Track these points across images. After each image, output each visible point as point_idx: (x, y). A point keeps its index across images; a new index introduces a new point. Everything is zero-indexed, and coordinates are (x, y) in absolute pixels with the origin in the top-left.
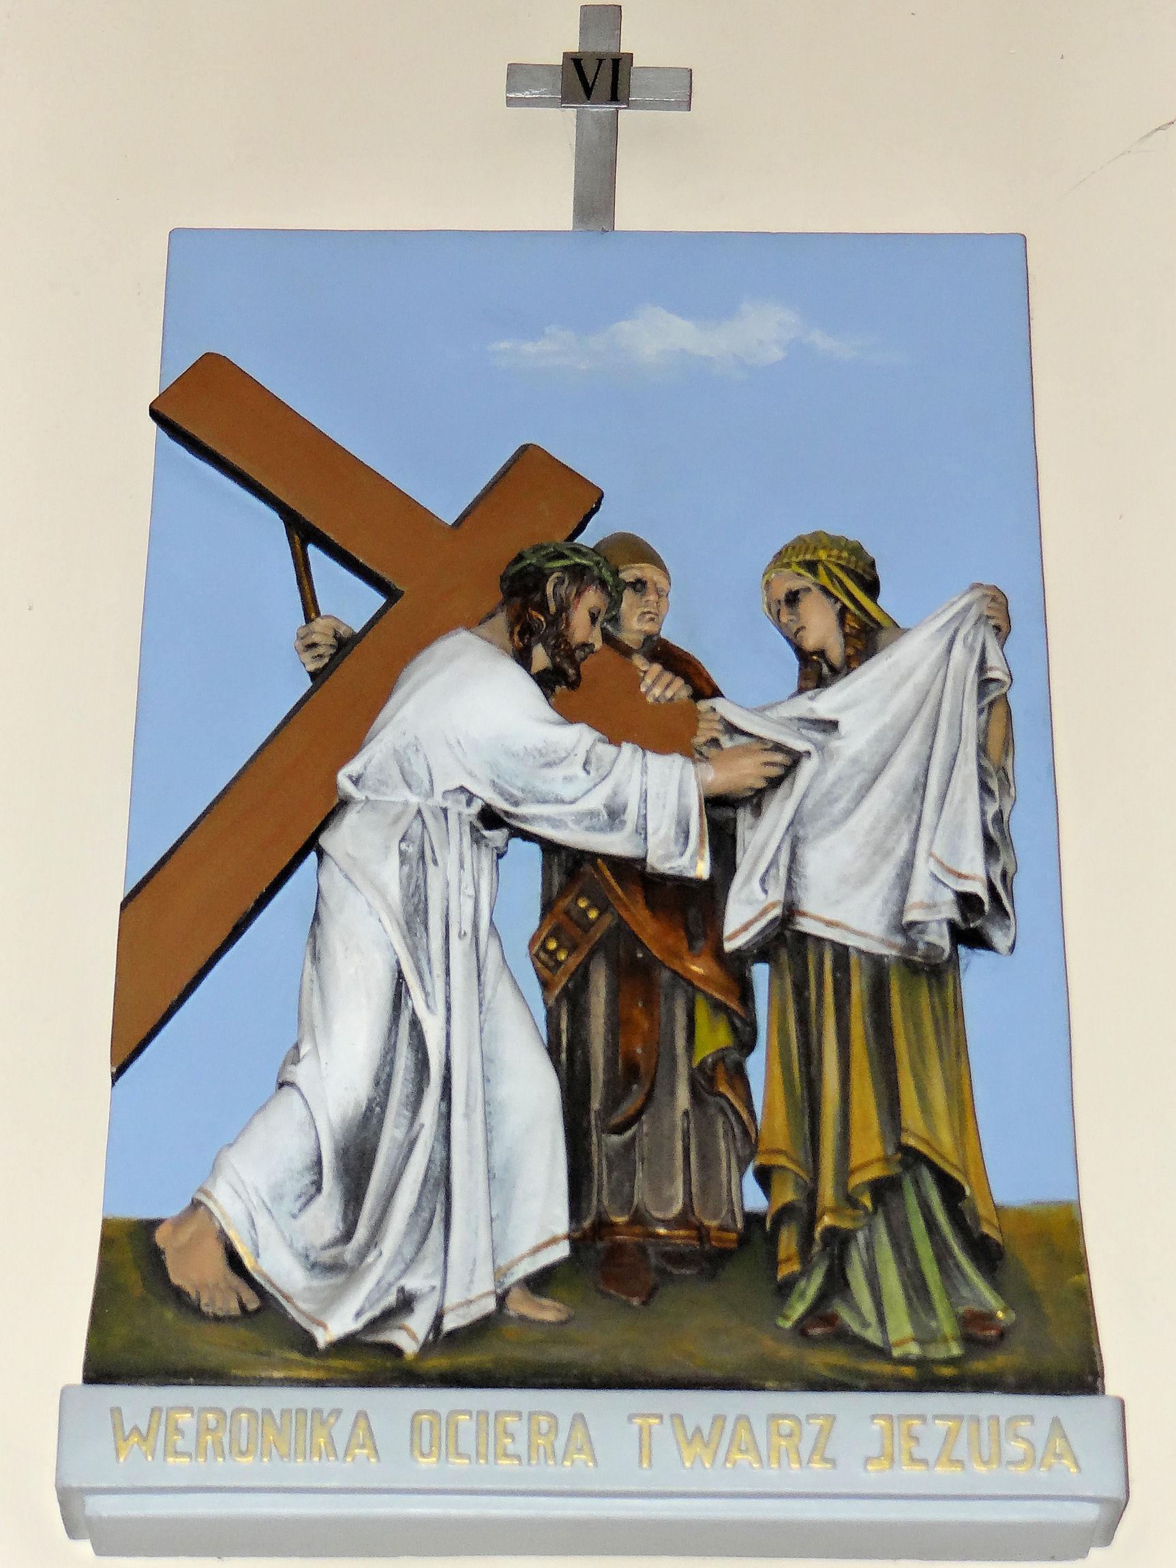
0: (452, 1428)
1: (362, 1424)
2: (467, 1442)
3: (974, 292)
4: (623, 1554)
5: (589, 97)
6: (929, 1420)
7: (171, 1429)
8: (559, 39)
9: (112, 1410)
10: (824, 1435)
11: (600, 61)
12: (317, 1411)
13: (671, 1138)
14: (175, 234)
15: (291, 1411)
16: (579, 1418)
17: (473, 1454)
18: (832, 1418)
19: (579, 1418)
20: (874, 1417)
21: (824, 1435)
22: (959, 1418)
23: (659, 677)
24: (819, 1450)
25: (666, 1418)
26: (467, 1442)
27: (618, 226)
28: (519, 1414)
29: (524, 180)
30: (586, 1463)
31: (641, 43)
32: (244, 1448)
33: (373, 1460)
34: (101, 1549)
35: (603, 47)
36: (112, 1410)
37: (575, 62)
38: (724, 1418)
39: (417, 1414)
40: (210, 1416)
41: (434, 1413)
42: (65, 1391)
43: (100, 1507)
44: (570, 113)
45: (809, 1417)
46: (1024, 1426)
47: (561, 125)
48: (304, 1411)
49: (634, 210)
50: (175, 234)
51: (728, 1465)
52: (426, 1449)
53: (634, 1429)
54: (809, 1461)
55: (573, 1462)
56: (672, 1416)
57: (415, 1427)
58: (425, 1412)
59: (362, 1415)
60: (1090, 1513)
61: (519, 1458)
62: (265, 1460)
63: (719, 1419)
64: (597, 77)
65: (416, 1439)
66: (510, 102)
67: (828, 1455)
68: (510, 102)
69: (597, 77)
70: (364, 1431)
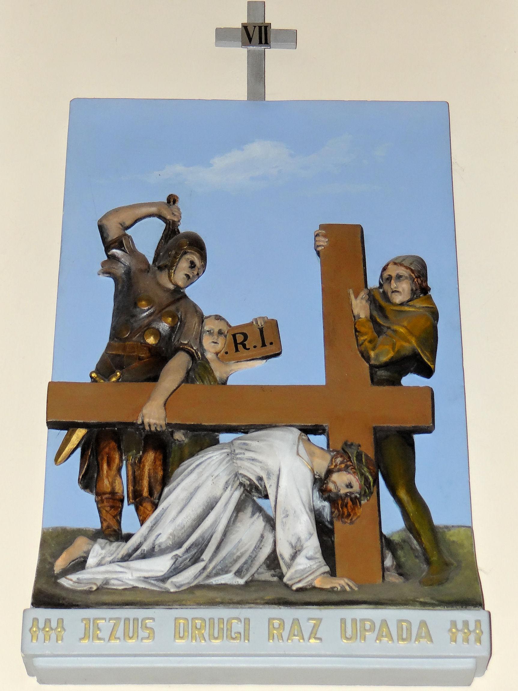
1: (48, 624)
7: (194, 628)
8: (238, 19)
9: (342, 619)
10: (315, 628)
11: (255, 27)
12: (136, 620)
15: (89, 620)
17: (122, 638)
18: (320, 620)
19: (296, 621)
20: (310, 619)
21: (315, 628)
22: (118, 619)
24: (313, 634)
29: (225, 76)
31: (275, 20)
32: (181, 635)
33: (301, 641)
34: (41, 681)
35: (259, 21)
36: (342, 619)
37: (245, 27)
40: (181, 621)
41: (186, 619)
42: (25, 611)
43: (40, 662)
44: (244, 51)
47: (240, 54)
48: (129, 619)
49: (276, 89)
51: (378, 641)
52: (216, 635)
53: (83, 624)
54: (309, 639)
55: (292, 640)
57: (176, 627)
58: (277, 619)
59: (296, 621)
60: (469, 664)
64: (257, 34)
67: (317, 636)
69: (257, 34)
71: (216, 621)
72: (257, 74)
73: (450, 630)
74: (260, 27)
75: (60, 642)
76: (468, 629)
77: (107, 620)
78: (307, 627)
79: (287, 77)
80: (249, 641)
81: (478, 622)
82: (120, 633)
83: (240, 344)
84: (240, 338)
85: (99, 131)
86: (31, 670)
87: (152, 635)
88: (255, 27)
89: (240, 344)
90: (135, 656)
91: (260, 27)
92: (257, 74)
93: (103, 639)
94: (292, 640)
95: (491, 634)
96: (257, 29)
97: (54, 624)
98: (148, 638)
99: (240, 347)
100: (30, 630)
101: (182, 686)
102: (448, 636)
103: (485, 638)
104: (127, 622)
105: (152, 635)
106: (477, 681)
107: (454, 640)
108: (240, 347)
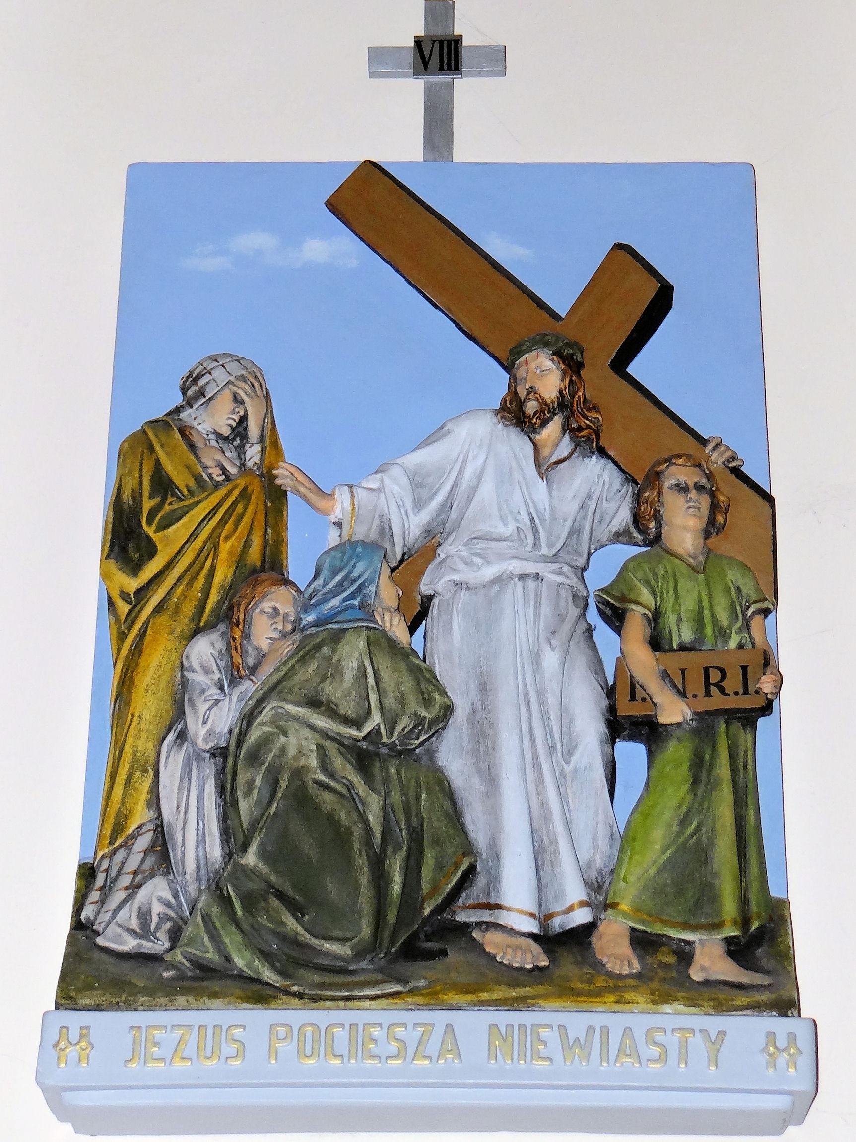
0: (329, 1037)
2: (342, 1046)
3: (735, 186)
4: (470, 1131)
5: (426, 69)
6: (169, 1028)
7: (367, 1039)
8: (409, 26)
11: (434, 41)
13: (284, 796)
14: (746, 173)
16: (449, 1027)
17: (194, 1057)
19: (449, 1027)
23: (234, 420)
25: (556, 1029)
26: (342, 1046)
27: (456, 159)
28: (343, 1025)
30: (633, 1064)
31: (470, 28)
33: (637, 1065)
35: (439, 32)
36: (62, 1027)
38: (357, 1025)
39: (304, 1025)
45: (673, 1030)
46: (237, 1032)
47: (412, 91)
49: (466, 149)
50: (746, 173)
52: (308, 1052)
55: (622, 1063)
56: (559, 1026)
58: (312, 1025)
60: (780, 1103)
61: (430, 1058)
62: (353, 1061)
63: (591, 1029)
64: (440, 54)
65: (302, 1045)
66: (372, 75)
68: (372, 75)
69: (440, 54)
70: (451, 1043)
71: (224, 1029)
72: (438, 124)
73: (764, 1050)
74: (441, 42)
75: (493, 1062)
76: (776, 1047)
77: (169, 1028)
78: (412, 1036)
79: (491, 123)
80: (686, 1064)
81: (792, 1038)
82: (190, 1049)
83: (714, 684)
84: (715, 676)
85: (167, 207)
86: (60, 1108)
87: (241, 1052)
88: (434, 41)
89: (714, 684)
90: (131, 1087)
91: (441, 42)
92: (438, 124)
93: (163, 1059)
94: (622, 1063)
95: (817, 1053)
96: (437, 44)
97: (781, 1043)
98: (655, 1061)
99: (714, 690)
100: (54, 1046)
101: (408, 1134)
102: (763, 1059)
103: (805, 1061)
104: (218, 1031)
105: (241, 1052)
106: (791, 1130)
107: (772, 1062)
108: (714, 690)
